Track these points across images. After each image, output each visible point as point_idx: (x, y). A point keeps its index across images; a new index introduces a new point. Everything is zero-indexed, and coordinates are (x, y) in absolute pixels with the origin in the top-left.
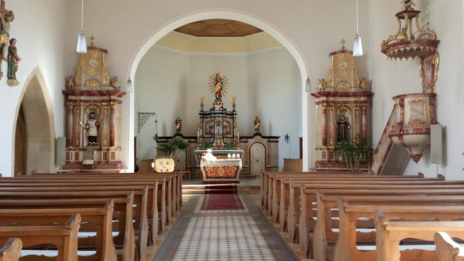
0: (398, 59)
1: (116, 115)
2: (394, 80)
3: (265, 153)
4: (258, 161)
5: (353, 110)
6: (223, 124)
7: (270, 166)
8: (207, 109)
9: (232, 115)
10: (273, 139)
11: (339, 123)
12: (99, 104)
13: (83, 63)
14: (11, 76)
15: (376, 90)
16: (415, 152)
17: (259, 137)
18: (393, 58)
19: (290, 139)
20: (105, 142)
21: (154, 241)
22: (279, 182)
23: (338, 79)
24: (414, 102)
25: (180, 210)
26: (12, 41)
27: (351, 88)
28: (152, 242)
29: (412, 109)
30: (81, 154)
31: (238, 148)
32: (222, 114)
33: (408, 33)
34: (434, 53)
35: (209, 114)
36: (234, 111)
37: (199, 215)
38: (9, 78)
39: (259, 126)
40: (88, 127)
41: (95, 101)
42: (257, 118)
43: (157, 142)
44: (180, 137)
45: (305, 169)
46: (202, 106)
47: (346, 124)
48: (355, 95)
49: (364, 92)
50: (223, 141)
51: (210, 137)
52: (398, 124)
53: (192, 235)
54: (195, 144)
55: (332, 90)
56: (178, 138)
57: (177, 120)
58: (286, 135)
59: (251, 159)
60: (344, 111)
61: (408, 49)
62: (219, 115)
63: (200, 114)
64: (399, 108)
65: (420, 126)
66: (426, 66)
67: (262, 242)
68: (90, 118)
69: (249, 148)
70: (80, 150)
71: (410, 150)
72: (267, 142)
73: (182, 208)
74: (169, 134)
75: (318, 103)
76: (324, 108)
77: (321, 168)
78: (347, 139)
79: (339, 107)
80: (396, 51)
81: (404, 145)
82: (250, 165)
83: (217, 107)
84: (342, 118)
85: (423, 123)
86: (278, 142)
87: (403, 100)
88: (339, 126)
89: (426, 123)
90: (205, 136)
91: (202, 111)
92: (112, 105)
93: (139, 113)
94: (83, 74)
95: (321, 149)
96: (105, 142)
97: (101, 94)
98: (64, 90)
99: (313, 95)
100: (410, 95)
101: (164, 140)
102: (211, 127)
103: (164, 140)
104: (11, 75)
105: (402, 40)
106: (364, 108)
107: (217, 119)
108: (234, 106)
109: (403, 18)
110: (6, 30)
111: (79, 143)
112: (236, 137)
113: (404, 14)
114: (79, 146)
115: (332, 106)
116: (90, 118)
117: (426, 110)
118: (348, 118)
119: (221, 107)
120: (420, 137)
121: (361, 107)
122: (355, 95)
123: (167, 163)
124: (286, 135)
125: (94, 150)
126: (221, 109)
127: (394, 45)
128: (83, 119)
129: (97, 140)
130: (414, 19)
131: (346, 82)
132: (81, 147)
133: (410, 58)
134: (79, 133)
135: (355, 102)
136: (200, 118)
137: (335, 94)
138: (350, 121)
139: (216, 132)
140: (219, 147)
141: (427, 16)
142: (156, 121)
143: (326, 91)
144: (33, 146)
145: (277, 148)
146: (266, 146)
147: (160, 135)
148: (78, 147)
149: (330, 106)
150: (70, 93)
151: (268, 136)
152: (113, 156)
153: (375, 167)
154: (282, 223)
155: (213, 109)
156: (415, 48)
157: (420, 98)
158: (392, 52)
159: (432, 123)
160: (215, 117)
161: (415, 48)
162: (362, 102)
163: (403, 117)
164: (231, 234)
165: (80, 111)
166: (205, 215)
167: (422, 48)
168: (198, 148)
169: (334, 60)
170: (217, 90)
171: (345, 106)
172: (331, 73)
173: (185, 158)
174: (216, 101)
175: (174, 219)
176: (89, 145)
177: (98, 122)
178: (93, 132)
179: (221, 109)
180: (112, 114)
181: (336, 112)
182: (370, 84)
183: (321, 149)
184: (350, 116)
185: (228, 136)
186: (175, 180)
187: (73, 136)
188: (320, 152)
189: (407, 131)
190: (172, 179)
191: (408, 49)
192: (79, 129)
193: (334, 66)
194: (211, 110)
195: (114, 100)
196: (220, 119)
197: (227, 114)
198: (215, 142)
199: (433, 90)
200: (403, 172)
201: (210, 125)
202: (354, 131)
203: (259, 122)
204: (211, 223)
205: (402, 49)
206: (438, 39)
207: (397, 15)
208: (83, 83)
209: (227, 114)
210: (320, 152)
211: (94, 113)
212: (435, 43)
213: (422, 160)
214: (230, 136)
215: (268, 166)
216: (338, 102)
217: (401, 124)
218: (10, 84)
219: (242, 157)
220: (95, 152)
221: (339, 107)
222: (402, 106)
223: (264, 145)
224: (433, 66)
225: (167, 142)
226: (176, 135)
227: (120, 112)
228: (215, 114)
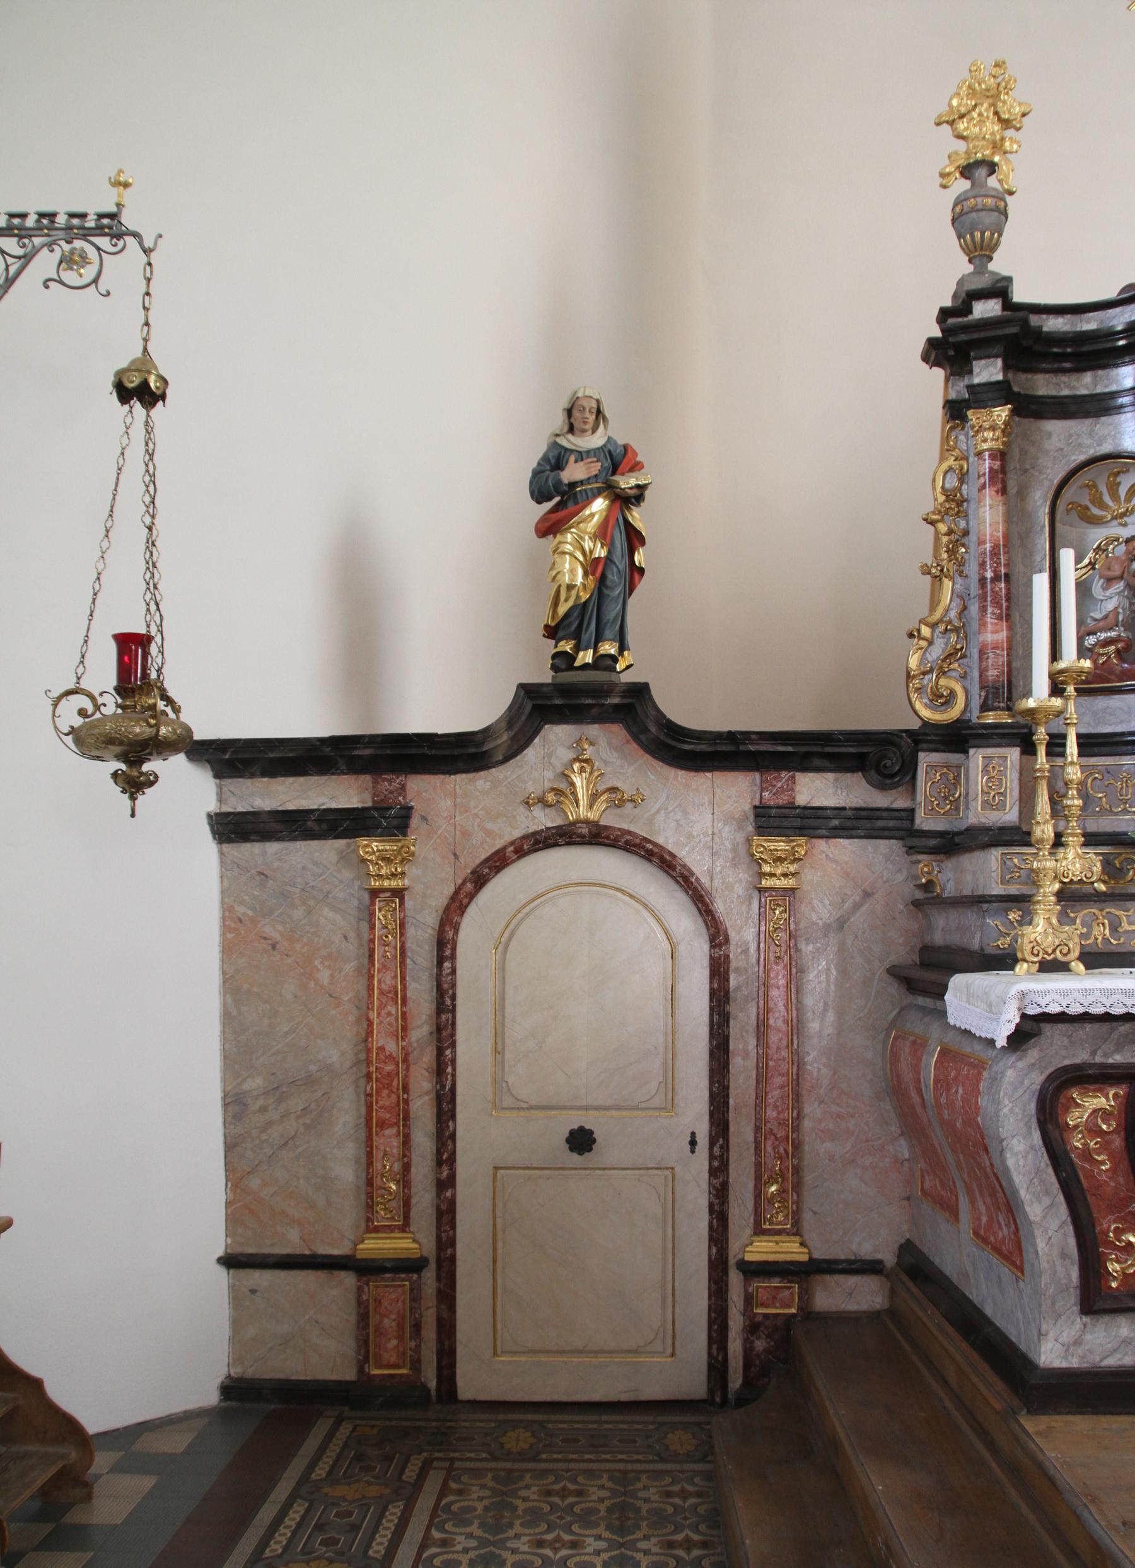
7: (789, 1250)
44: (606, 743)
56: (580, 765)
57: (556, 459)
74: (443, 688)
101: (342, 793)
103: (342, 793)
142: (139, 391)
173: (695, 1112)
223: (685, 880)
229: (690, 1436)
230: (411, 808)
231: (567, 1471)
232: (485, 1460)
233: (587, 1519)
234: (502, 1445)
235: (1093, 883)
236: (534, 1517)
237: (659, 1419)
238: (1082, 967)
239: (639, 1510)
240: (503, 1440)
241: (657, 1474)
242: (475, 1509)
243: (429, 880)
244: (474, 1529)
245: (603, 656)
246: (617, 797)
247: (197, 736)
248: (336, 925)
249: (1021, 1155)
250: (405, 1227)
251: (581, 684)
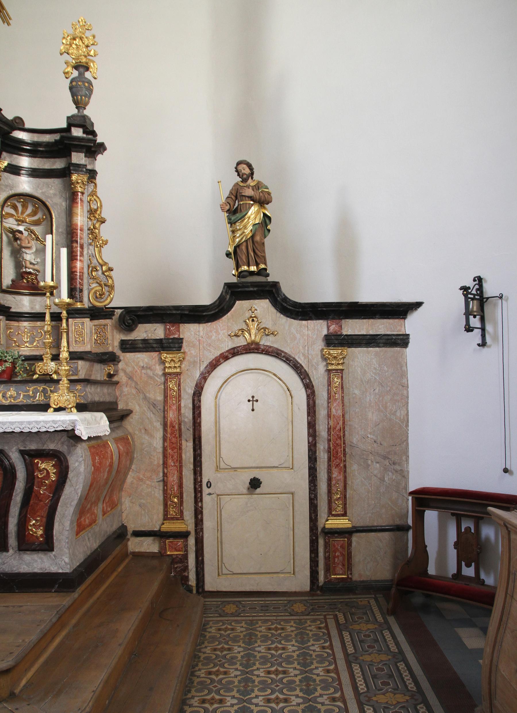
3: (312, 425)
4: (255, 484)
10: (366, 323)
17: (263, 306)
42: (245, 171)
58: (469, 283)
69: (188, 389)
72: (320, 344)
82: (198, 513)
86: (402, 341)
124: (469, 283)
215: (334, 523)
223: (297, 367)
229: (303, 605)
230: (409, 335)
231: (227, 621)
232: (217, 617)
233: (287, 638)
234: (224, 611)
235: (52, 375)
236: (265, 638)
237: (223, 600)
238: (75, 411)
239: (308, 634)
240: (224, 609)
241: (314, 621)
242: (240, 636)
244: (241, 644)
245: (242, 272)
246: (265, 331)
247: (12, 310)
250: (345, 515)
251: (250, 284)
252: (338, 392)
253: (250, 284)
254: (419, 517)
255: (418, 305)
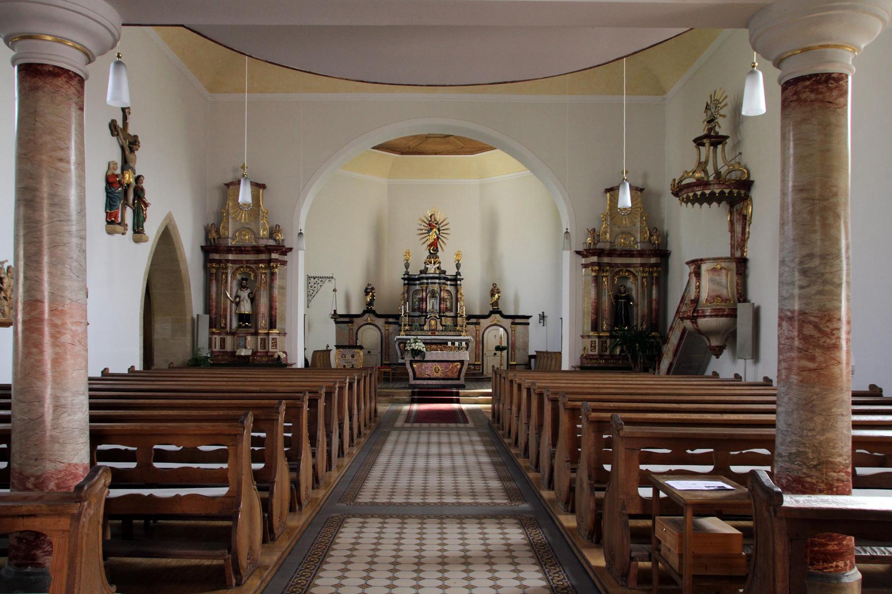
0: (697, 205)
1: (277, 283)
2: (696, 233)
5: (639, 278)
6: (440, 295)
8: (414, 271)
9: (455, 280)
11: (617, 298)
12: (253, 266)
13: (231, 204)
14: (138, 229)
15: (672, 246)
16: (714, 342)
17: (498, 316)
18: (689, 204)
19: (548, 320)
20: (263, 322)
21: (346, 452)
22: (511, 382)
23: (617, 230)
24: (714, 269)
25: (375, 421)
26: (138, 179)
27: (636, 243)
28: (343, 453)
29: (712, 281)
30: (229, 339)
31: (464, 334)
32: (439, 278)
33: (710, 169)
34: (746, 198)
35: (419, 279)
36: (458, 274)
37: (402, 429)
38: (135, 232)
39: (498, 298)
40: (238, 300)
41: (248, 261)
42: (494, 285)
43: (336, 323)
45: (565, 366)
46: (407, 266)
47: (629, 298)
48: (641, 254)
49: (655, 250)
50: (441, 322)
51: (419, 316)
52: (692, 301)
53: (388, 464)
54: (396, 326)
55: (607, 247)
56: (369, 318)
57: (367, 289)
59: (485, 352)
60: (626, 278)
61: (707, 192)
62: (434, 281)
63: (404, 279)
64: (694, 279)
65: (723, 306)
66: (736, 217)
67: (485, 459)
68: (242, 287)
70: (227, 334)
71: (709, 340)
73: (378, 419)
74: (356, 310)
75: (585, 266)
76: (594, 274)
77: (586, 366)
78: (628, 323)
79: (617, 273)
80: (691, 194)
81: (699, 332)
83: (432, 268)
84: (622, 289)
85: (726, 300)
86: (528, 324)
87: (699, 267)
88: (617, 302)
89: (730, 300)
90: (412, 314)
91: (407, 273)
92: (273, 267)
93: (309, 278)
94: (230, 220)
95: (589, 337)
96: (263, 322)
97: (257, 250)
98: (203, 244)
99: (578, 253)
100: (708, 259)
102: (422, 300)
104: (138, 227)
105: (698, 180)
106: (655, 275)
107: (431, 287)
108: (458, 266)
109: (703, 145)
110: (131, 165)
111: (226, 324)
112: (461, 316)
113: (705, 141)
114: (225, 328)
115: (607, 271)
116: (242, 287)
117: (732, 281)
118: (630, 289)
119: (438, 268)
120: (721, 321)
121: (651, 273)
122: (641, 254)
123: (353, 356)
125: (248, 334)
126: (438, 272)
127: (689, 186)
128: (232, 287)
129: (251, 320)
130: (720, 147)
131: (630, 234)
132: (228, 329)
133: (715, 204)
134: (225, 310)
135: (642, 265)
136: (405, 284)
137: (611, 253)
138: (634, 294)
139: (429, 307)
140: (433, 332)
141: (737, 144)
142: (335, 290)
143: (598, 247)
144: (162, 328)
145: (526, 334)
146: (509, 331)
147: (341, 311)
148: (224, 330)
149: (603, 271)
150: (212, 249)
151: (512, 314)
152: (275, 345)
153: (665, 364)
154: (507, 430)
155: (425, 271)
156: (717, 191)
157: (723, 264)
158: (685, 196)
159: (740, 302)
160: (427, 283)
161: (717, 191)
162: (652, 265)
163: (699, 292)
164: (447, 463)
165: (227, 277)
166: (410, 429)
167: (727, 191)
168: (402, 333)
169: (610, 200)
170: (431, 241)
171: (627, 271)
172: (606, 220)
174: (429, 257)
175: (368, 432)
176: (239, 326)
177: (251, 293)
178: (246, 308)
179: (438, 272)
180: (272, 280)
181: (613, 280)
182: (664, 238)
183: (589, 337)
184: (633, 286)
185: (447, 314)
186: (368, 379)
187: (216, 314)
188: (588, 342)
189: (703, 311)
190: (365, 377)
191: (707, 192)
192: (225, 303)
193: (610, 209)
194: (421, 272)
195: (276, 260)
196: (436, 287)
197: (447, 279)
198: (427, 323)
199: (743, 252)
200: (705, 370)
201: (420, 296)
202: (640, 308)
203: (498, 293)
204: (426, 480)
205: (699, 193)
206: (751, 179)
207: (695, 141)
208: (230, 236)
209: (447, 279)
210: (588, 342)
211: (246, 280)
212: (746, 185)
213: (726, 354)
214: (452, 314)
216: (616, 265)
217: (696, 301)
218: (136, 241)
219: (470, 349)
220: (249, 338)
221: (617, 273)
222: (698, 274)
224: (745, 217)
225: (351, 322)
226: (365, 312)
227: (284, 277)
228: (427, 278)
243: (355, 327)
248: (346, 332)
249: (397, 347)
251: (369, 310)
252: (514, 335)
253: (496, 311)
254: (530, 361)
255: (374, 148)
